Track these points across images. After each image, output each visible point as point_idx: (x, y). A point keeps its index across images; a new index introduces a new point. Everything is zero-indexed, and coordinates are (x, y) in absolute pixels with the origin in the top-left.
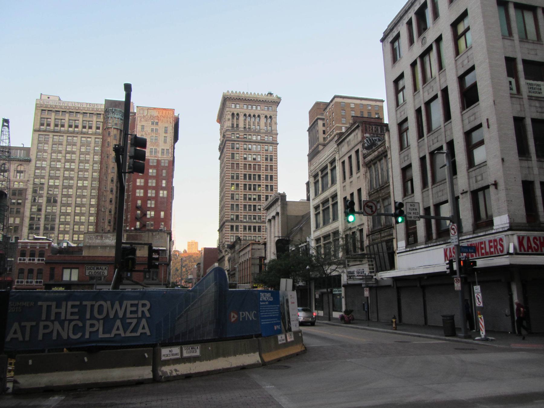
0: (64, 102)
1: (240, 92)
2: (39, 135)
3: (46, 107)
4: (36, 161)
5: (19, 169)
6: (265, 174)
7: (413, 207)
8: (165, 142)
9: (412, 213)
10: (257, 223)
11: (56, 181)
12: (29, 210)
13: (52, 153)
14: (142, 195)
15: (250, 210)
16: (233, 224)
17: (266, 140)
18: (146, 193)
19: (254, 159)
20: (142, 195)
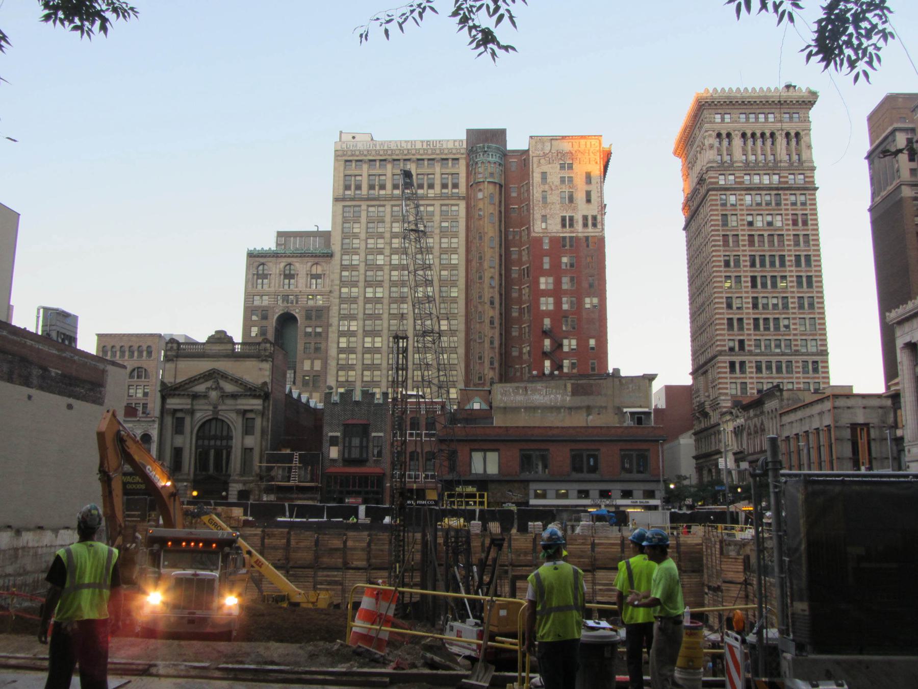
0: (382, 144)
1: (730, 89)
2: (344, 206)
3: (352, 155)
4: (342, 255)
5: (314, 272)
6: (793, 253)
10: (783, 354)
11: (378, 290)
12: (336, 346)
13: (367, 238)
14: (551, 307)
15: (767, 329)
16: (733, 358)
17: (722, 182)
18: (558, 304)
19: (770, 224)
20: (551, 307)
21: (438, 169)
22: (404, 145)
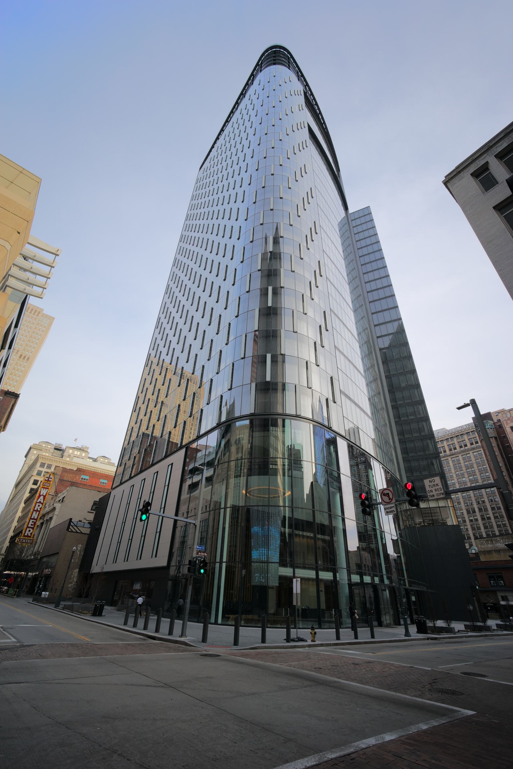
7: (433, 483)
9: (434, 491)
21: (466, 437)
22: (458, 429)
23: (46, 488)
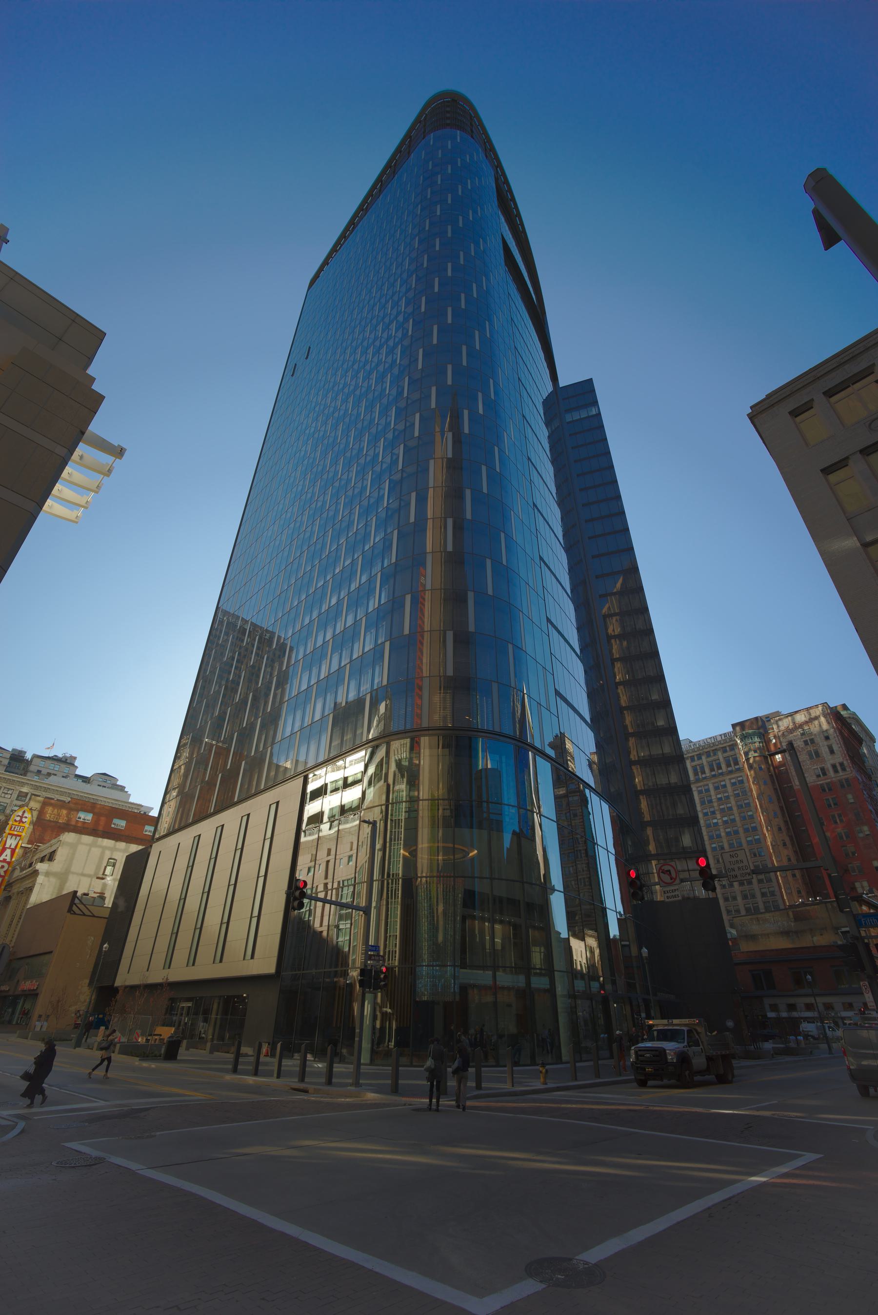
7: (735, 859)
8: (832, 752)
21: (704, 760)
22: (709, 741)
23: (16, 836)
